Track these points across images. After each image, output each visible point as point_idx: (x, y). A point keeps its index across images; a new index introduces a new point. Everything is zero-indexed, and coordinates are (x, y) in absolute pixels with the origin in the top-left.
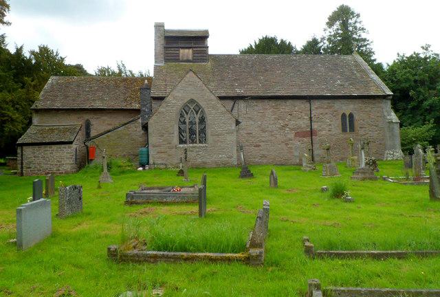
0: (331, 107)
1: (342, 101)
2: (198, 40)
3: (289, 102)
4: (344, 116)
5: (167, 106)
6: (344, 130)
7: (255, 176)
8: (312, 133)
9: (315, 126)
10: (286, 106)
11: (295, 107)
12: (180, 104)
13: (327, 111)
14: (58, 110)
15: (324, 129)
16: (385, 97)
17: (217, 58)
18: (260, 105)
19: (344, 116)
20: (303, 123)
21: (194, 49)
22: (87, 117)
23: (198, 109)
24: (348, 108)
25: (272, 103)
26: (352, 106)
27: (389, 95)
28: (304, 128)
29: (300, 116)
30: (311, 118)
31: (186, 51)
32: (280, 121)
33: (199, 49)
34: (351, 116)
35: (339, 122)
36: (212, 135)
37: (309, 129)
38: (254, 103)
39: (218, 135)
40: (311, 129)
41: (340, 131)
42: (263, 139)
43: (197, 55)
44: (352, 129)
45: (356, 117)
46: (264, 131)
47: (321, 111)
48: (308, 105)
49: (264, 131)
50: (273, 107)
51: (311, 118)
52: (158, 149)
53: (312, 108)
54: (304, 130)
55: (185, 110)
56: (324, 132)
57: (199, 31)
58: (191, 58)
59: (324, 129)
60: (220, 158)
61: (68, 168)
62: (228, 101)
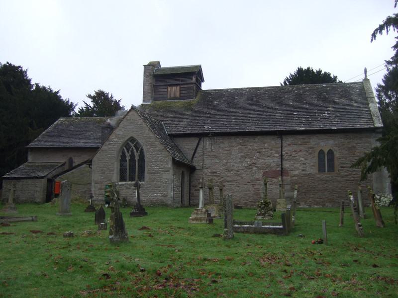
0: (305, 143)
1: (321, 136)
2: (194, 74)
3: (257, 139)
4: (321, 152)
5: (110, 144)
6: (321, 169)
7: (148, 214)
8: (282, 172)
9: (287, 165)
10: (254, 144)
11: (265, 143)
12: (121, 141)
13: (302, 148)
14: (47, 149)
15: (297, 169)
16: (374, 130)
17: (208, 93)
18: (226, 143)
19: (321, 152)
20: (273, 161)
21: (182, 86)
22: (71, 155)
23: (137, 146)
24: (326, 144)
25: (240, 140)
26: (331, 142)
27: (379, 128)
28: (274, 166)
29: (269, 154)
30: (282, 155)
31: (174, 88)
32: (247, 160)
33: (185, 86)
34: (331, 152)
35: (316, 160)
36: (148, 173)
37: (279, 169)
38: (219, 140)
39: (154, 173)
40: (282, 168)
41: (316, 168)
42: (228, 179)
43: (184, 92)
44: (331, 168)
45: (337, 154)
46: (229, 170)
47: (291, 148)
48: (279, 141)
49: (229, 170)
50: (240, 143)
51: (282, 155)
52: (99, 186)
53: (284, 145)
54: (274, 169)
55: (126, 145)
56: (297, 172)
57: (182, 68)
58: (178, 95)
59: (297, 169)
60: (156, 196)
61: (38, 200)
62: (193, 139)
